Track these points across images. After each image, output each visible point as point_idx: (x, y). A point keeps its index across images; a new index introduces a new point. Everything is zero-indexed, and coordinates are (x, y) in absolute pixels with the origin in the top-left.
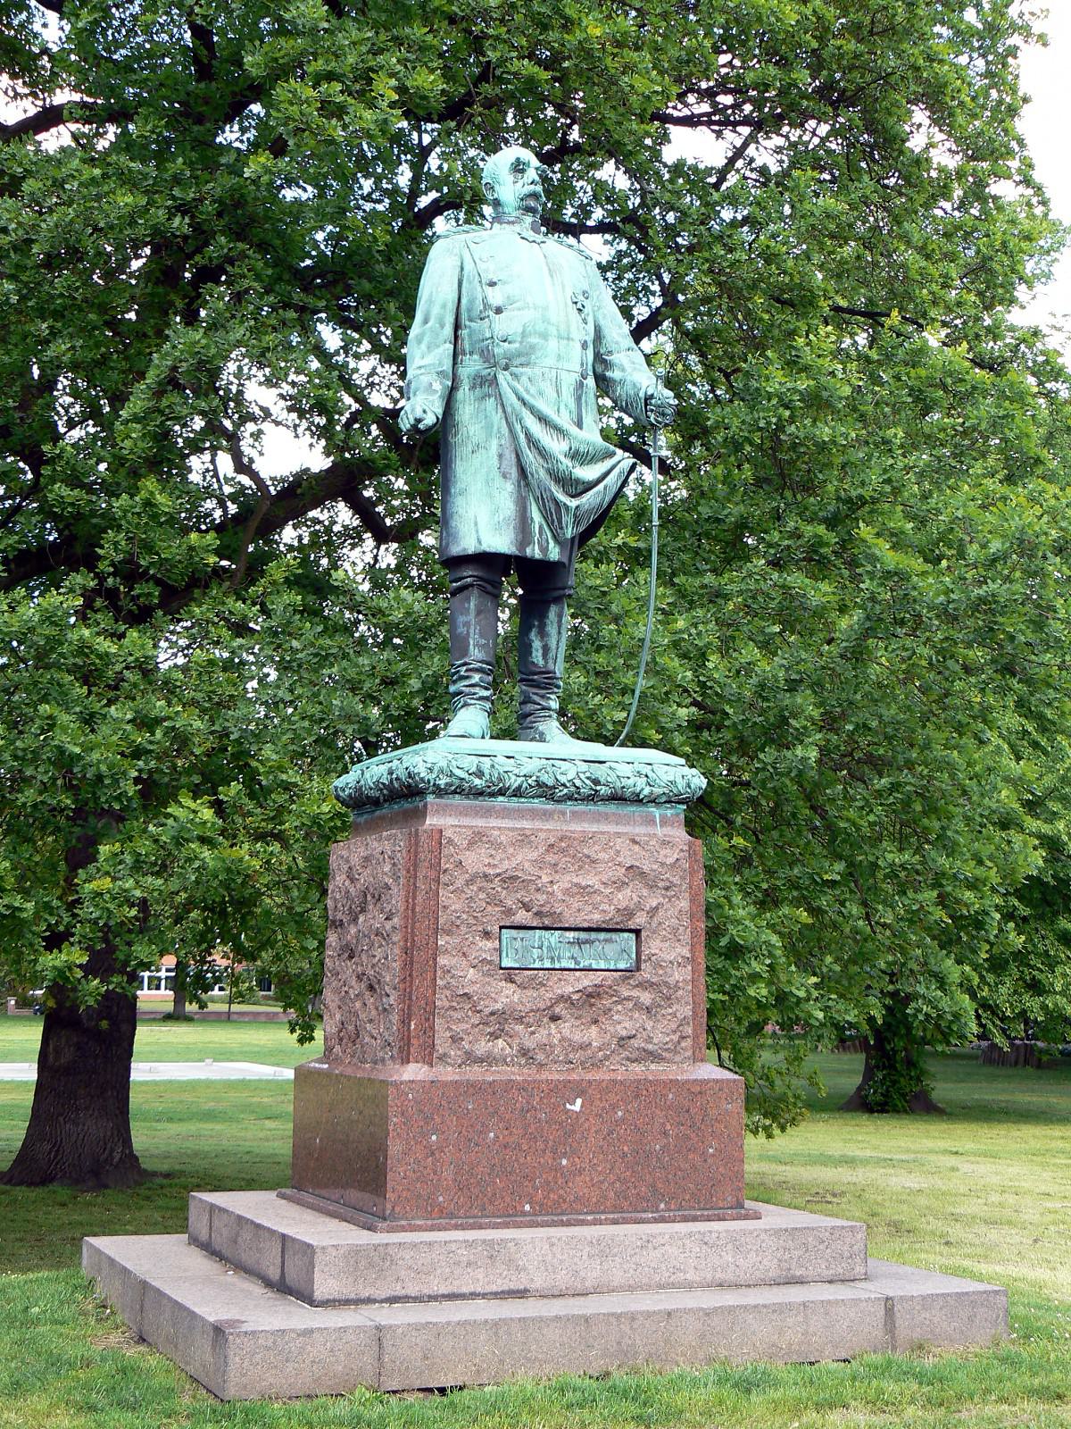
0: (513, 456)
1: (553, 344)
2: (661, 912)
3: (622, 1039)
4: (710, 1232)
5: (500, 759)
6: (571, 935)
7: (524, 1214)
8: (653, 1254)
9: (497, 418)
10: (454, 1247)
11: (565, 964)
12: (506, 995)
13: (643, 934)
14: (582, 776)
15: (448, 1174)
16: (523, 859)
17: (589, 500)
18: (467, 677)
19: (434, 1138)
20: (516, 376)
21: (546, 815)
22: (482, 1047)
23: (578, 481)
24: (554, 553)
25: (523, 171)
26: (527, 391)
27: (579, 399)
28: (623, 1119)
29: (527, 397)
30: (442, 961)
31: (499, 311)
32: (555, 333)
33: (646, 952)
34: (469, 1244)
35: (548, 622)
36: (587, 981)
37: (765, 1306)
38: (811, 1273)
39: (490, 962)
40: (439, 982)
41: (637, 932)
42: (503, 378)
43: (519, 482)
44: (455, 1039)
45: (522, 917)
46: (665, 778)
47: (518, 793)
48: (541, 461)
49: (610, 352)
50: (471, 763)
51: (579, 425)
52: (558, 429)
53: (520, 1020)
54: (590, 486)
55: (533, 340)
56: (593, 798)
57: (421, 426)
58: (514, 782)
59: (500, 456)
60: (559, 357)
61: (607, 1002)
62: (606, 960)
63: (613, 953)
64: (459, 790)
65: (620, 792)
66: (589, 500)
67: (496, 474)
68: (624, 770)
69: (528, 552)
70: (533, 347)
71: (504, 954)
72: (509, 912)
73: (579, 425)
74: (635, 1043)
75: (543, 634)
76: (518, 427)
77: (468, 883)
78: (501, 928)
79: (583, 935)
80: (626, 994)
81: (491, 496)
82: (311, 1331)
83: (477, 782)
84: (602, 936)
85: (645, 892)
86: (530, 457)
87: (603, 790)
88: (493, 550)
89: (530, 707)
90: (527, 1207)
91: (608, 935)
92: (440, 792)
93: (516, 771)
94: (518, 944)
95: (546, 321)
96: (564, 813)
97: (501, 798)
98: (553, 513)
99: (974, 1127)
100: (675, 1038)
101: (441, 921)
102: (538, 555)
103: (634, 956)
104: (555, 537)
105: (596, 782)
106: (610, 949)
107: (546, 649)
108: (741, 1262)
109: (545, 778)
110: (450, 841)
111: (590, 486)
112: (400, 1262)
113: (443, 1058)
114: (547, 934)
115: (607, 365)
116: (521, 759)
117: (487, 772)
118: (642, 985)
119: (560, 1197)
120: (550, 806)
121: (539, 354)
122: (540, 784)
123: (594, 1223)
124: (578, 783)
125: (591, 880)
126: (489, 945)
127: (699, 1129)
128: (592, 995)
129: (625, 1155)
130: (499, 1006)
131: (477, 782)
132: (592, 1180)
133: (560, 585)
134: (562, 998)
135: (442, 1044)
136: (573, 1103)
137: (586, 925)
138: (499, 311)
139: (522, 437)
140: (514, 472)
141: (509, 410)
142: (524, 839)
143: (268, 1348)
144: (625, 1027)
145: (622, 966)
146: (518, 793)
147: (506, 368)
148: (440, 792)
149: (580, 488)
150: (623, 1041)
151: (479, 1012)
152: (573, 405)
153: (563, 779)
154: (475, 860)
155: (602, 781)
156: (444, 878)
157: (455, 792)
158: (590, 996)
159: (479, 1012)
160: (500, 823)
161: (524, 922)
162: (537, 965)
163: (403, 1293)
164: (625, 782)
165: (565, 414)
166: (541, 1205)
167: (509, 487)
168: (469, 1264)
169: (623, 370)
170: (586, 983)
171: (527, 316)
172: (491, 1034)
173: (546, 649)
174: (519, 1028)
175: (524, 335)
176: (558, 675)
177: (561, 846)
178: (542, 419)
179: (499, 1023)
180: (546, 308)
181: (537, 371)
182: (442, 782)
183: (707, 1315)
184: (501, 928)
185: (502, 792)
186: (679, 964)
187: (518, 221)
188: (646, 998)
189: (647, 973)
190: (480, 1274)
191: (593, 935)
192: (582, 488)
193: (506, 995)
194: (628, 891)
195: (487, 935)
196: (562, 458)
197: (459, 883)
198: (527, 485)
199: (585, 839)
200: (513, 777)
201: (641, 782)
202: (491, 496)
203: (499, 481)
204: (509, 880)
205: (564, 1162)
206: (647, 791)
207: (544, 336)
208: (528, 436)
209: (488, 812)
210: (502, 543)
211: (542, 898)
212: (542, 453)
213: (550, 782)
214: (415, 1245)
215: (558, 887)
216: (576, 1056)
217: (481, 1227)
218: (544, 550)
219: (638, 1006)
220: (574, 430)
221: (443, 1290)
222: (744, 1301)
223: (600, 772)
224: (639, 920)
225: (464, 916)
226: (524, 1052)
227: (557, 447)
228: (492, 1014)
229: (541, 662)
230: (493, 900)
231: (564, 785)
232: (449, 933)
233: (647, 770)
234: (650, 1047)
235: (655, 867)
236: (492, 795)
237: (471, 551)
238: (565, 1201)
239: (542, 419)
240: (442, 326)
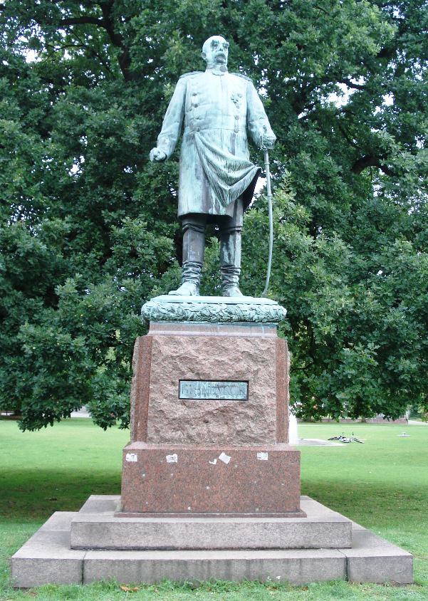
0: (201, 169)
1: (219, 118)
2: (260, 373)
3: (238, 431)
4: (268, 523)
5: (185, 304)
6: (214, 384)
7: (188, 511)
8: (238, 532)
9: (195, 152)
10: (138, 525)
11: (211, 397)
12: (180, 411)
13: (250, 383)
14: (223, 311)
15: (151, 491)
16: (191, 349)
17: (237, 186)
18: (187, 269)
19: (144, 475)
20: (202, 134)
21: (207, 329)
22: (170, 434)
23: (231, 178)
24: (223, 211)
25: (216, 46)
26: (207, 140)
27: (233, 141)
28: (238, 469)
29: (206, 142)
30: (152, 395)
31: (196, 106)
32: (221, 113)
33: (251, 391)
34: (145, 524)
35: (230, 243)
36: (221, 404)
37: (279, 560)
38: (321, 544)
39: (174, 396)
40: (150, 405)
41: (247, 382)
42: (197, 135)
43: (204, 180)
44: (157, 431)
45: (189, 375)
46: (265, 311)
47: (192, 319)
48: (214, 170)
49: (253, 120)
50: (168, 306)
51: (233, 153)
52: (222, 157)
53: (188, 422)
54: (237, 180)
55: (210, 117)
56: (230, 320)
57: (157, 159)
58: (190, 315)
59: (196, 170)
60: (222, 124)
61: (231, 414)
62: (232, 395)
63: (236, 392)
64: (164, 319)
65: (243, 318)
66: (237, 186)
67: (194, 178)
68: (245, 307)
69: (210, 211)
70: (210, 121)
71: (181, 392)
72: (183, 373)
73: (233, 153)
74: (245, 434)
75: (228, 249)
76: (203, 156)
77: (163, 360)
78: (180, 380)
79: (220, 384)
80: (240, 410)
81: (193, 188)
82: (51, 560)
83: (172, 314)
84: (230, 384)
85: (251, 363)
86: (208, 168)
87: (235, 317)
88: (193, 212)
89: (224, 282)
90: (189, 508)
91: (233, 383)
92: (155, 320)
93: (191, 309)
94: (188, 388)
95: (217, 108)
96: (216, 328)
97: (185, 322)
98: (220, 193)
99: (40, 472)
100: (266, 431)
101: (151, 377)
102: (215, 212)
103: (246, 393)
104: (223, 204)
105: (230, 313)
106: (234, 390)
107: (229, 255)
108: (284, 538)
109: (204, 312)
110: (156, 342)
111: (237, 180)
112: (112, 531)
113: (151, 439)
114: (202, 383)
115: (252, 126)
116: (216, 304)
117: (176, 310)
118: (251, 407)
119: (206, 504)
120: (209, 325)
121: (213, 123)
122: (203, 315)
123: (220, 516)
124: (221, 314)
125: (224, 359)
126: (174, 388)
127: (277, 474)
128: (223, 411)
129: (238, 486)
130: (177, 416)
131: (172, 314)
132: (221, 497)
133: (232, 226)
134: (210, 413)
135: (151, 434)
136: (213, 461)
137: (221, 379)
138: (196, 106)
139: (205, 160)
140: (202, 176)
141: (199, 149)
142: (193, 340)
143: (30, 566)
144: (240, 426)
145: (240, 397)
146: (192, 319)
147: (198, 131)
148: (155, 320)
149: (233, 181)
150: (239, 433)
151: (167, 418)
152: (229, 144)
153: (214, 312)
154: (167, 350)
155: (233, 312)
156: (153, 358)
157: (163, 319)
158: (222, 411)
159: (167, 418)
160: (182, 332)
161: (190, 378)
162: (197, 398)
163: (112, 545)
164: (246, 313)
165: (225, 149)
166: (196, 507)
167: (200, 183)
168: (146, 533)
169: (256, 127)
170: (220, 405)
171: (208, 107)
172: (174, 429)
173: (229, 255)
174: (187, 426)
175: (206, 115)
176: (236, 266)
177: (212, 342)
178: (214, 152)
179: (180, 424)
180: (217, 103)
181: (212, 131)
182: (155, 315)
183: (101, 562)
184: (180, 380)
185: (185, 319)
186: (269, 397)
187: (214, 67)
188: (251, 413)
189: (251, 401)
190: (150, 538)
191: (226, 383)
192: (230, 181)
193: (180, 411)
194: (242, 363)
195: (173, 383)
196: (223, 168)
197: (160, 360)
198: (209, 182)
199: (223, 339)
200: (189, 312)
201: (253, 313)
202: (193, 188)
203: (195, 180)
204: (183, 359)
205: (208, 488)
206: (256, 317)
207: (216, 115)
208: (208, 160)
209: (179, 329)
210: (196, 208)
211: (199, 367)
212: (214, 166)
213: (207, 314)
214: (119, 524)
215: (206, 362)
216: (215, 439)
217: (163, 517)
218: (218, 210)
219: (247, 416)
220: (229, 156)
221: (133, 544)
222: (316, 556)
223: (232, 308)
224: (249, 377)
225: (162, 375)
226: (190, 437)
227: (220, 163)
228: (174, 419)
229: (228, 261)
230: (176, 368)
231: (214, 315)
232: (155, 383)
233: (256, 307)
234: (253, 435)
235: (257, 352)
236: (180, 320)
237: (186, 213)
238: (208, 506)
239: (214, 152)
240: (174, 115)
